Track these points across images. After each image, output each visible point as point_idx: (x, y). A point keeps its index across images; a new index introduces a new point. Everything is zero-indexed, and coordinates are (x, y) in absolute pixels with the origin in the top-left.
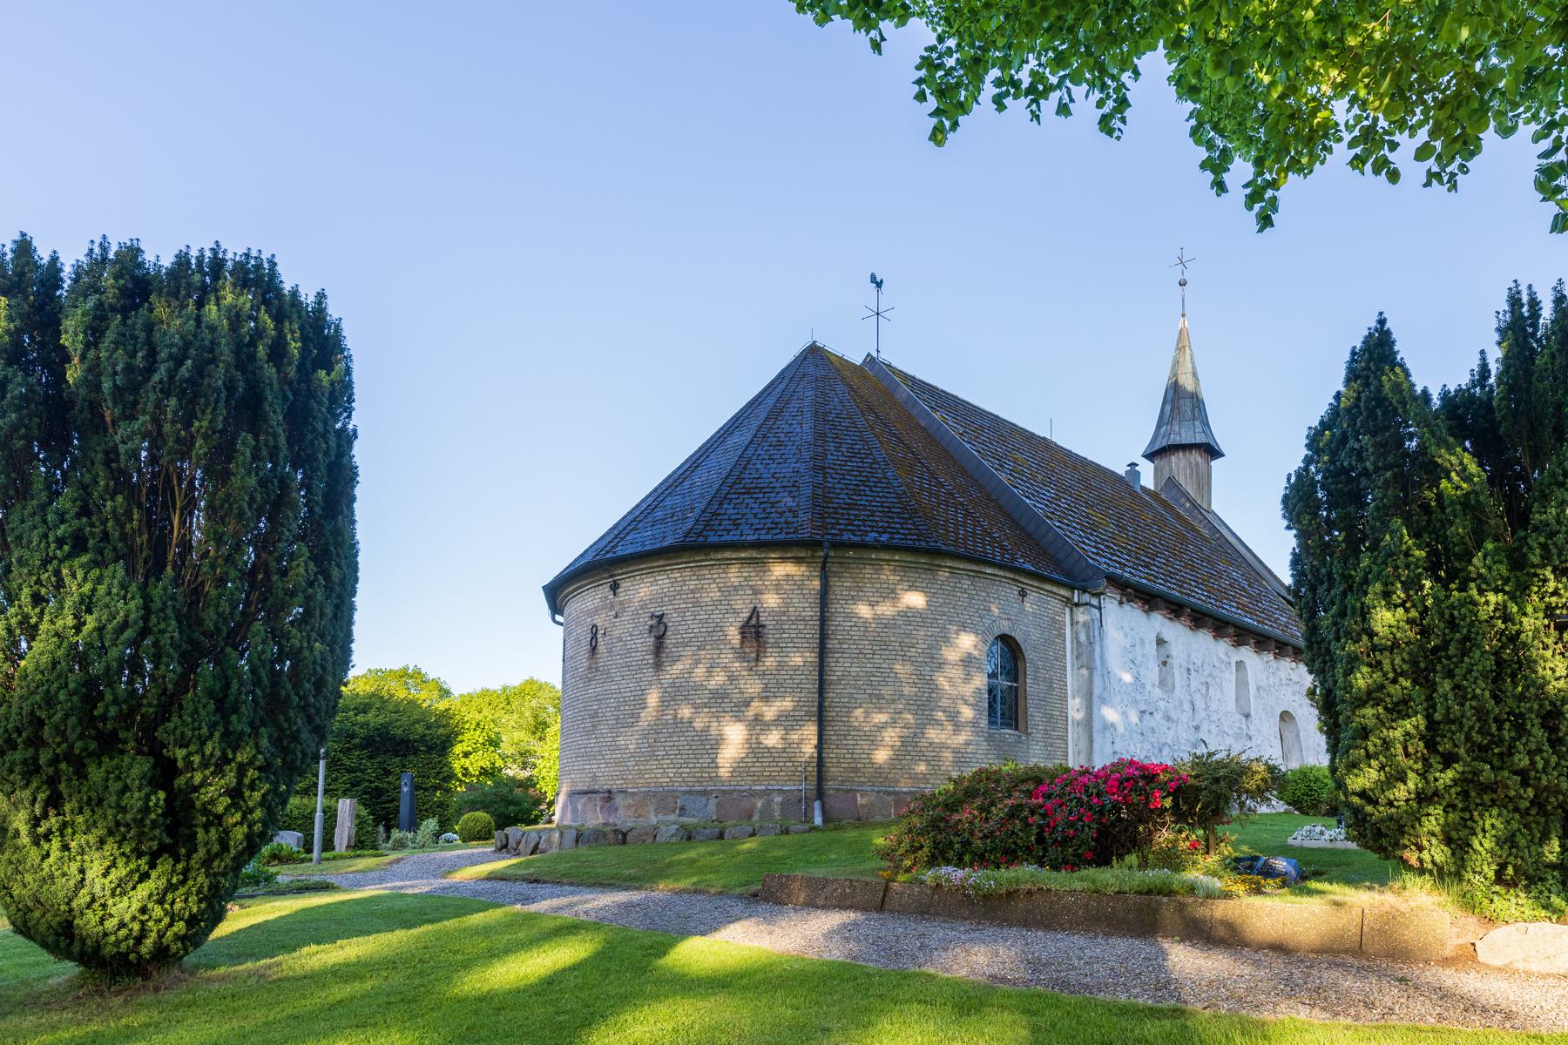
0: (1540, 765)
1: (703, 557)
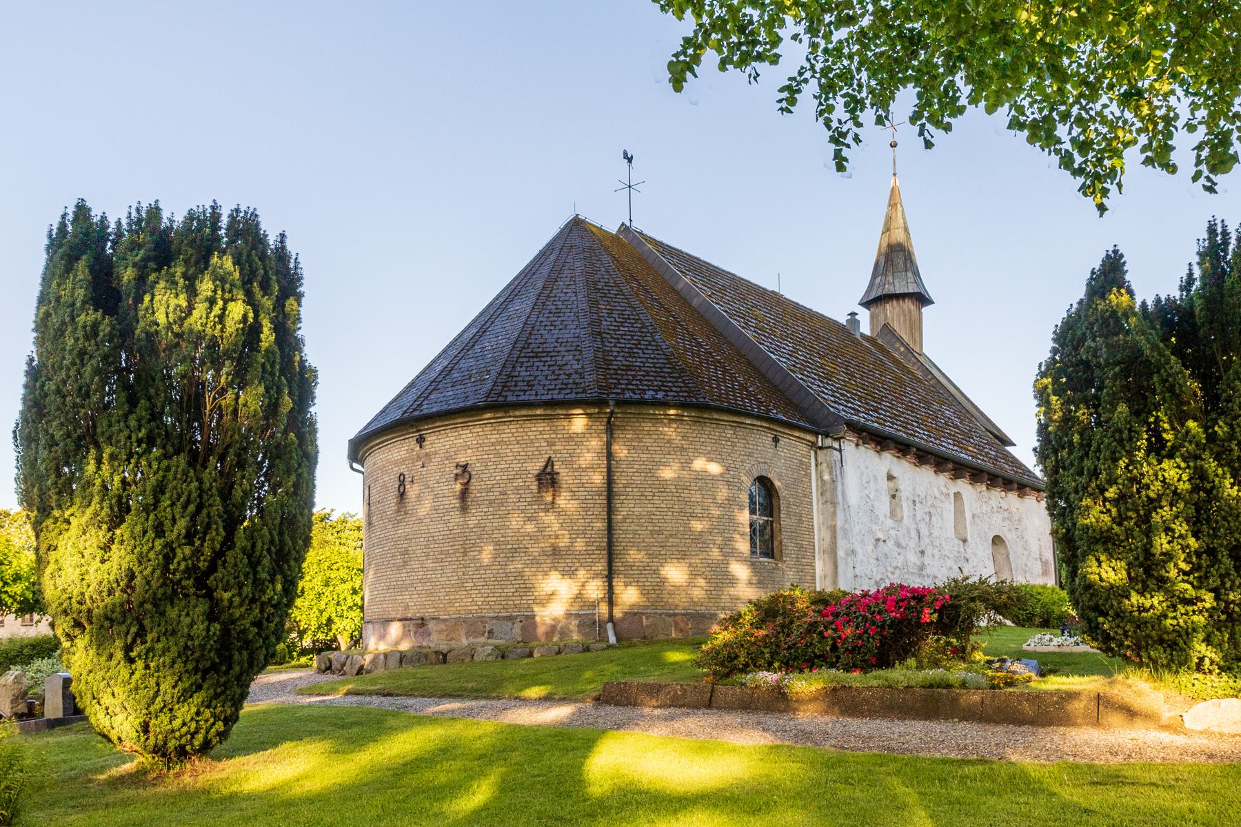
0: (1228, 585)
1: (492, 415)
